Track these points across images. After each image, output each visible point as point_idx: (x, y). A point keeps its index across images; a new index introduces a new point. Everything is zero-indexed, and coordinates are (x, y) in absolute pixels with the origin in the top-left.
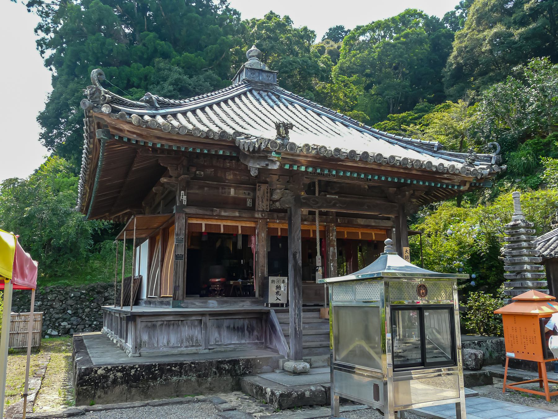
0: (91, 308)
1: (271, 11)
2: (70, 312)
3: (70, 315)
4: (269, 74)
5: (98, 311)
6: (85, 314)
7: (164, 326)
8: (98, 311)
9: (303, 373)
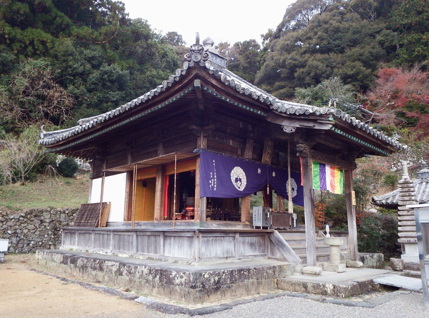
0: (28, 229)
1: (262, 36)
2: (9, 232)
3: (9, 234)
4: (221, 59)
5: (34, 232)
6: (23, 234)
7: (214, 241)
8: (34, 232)
9: (316, 274)
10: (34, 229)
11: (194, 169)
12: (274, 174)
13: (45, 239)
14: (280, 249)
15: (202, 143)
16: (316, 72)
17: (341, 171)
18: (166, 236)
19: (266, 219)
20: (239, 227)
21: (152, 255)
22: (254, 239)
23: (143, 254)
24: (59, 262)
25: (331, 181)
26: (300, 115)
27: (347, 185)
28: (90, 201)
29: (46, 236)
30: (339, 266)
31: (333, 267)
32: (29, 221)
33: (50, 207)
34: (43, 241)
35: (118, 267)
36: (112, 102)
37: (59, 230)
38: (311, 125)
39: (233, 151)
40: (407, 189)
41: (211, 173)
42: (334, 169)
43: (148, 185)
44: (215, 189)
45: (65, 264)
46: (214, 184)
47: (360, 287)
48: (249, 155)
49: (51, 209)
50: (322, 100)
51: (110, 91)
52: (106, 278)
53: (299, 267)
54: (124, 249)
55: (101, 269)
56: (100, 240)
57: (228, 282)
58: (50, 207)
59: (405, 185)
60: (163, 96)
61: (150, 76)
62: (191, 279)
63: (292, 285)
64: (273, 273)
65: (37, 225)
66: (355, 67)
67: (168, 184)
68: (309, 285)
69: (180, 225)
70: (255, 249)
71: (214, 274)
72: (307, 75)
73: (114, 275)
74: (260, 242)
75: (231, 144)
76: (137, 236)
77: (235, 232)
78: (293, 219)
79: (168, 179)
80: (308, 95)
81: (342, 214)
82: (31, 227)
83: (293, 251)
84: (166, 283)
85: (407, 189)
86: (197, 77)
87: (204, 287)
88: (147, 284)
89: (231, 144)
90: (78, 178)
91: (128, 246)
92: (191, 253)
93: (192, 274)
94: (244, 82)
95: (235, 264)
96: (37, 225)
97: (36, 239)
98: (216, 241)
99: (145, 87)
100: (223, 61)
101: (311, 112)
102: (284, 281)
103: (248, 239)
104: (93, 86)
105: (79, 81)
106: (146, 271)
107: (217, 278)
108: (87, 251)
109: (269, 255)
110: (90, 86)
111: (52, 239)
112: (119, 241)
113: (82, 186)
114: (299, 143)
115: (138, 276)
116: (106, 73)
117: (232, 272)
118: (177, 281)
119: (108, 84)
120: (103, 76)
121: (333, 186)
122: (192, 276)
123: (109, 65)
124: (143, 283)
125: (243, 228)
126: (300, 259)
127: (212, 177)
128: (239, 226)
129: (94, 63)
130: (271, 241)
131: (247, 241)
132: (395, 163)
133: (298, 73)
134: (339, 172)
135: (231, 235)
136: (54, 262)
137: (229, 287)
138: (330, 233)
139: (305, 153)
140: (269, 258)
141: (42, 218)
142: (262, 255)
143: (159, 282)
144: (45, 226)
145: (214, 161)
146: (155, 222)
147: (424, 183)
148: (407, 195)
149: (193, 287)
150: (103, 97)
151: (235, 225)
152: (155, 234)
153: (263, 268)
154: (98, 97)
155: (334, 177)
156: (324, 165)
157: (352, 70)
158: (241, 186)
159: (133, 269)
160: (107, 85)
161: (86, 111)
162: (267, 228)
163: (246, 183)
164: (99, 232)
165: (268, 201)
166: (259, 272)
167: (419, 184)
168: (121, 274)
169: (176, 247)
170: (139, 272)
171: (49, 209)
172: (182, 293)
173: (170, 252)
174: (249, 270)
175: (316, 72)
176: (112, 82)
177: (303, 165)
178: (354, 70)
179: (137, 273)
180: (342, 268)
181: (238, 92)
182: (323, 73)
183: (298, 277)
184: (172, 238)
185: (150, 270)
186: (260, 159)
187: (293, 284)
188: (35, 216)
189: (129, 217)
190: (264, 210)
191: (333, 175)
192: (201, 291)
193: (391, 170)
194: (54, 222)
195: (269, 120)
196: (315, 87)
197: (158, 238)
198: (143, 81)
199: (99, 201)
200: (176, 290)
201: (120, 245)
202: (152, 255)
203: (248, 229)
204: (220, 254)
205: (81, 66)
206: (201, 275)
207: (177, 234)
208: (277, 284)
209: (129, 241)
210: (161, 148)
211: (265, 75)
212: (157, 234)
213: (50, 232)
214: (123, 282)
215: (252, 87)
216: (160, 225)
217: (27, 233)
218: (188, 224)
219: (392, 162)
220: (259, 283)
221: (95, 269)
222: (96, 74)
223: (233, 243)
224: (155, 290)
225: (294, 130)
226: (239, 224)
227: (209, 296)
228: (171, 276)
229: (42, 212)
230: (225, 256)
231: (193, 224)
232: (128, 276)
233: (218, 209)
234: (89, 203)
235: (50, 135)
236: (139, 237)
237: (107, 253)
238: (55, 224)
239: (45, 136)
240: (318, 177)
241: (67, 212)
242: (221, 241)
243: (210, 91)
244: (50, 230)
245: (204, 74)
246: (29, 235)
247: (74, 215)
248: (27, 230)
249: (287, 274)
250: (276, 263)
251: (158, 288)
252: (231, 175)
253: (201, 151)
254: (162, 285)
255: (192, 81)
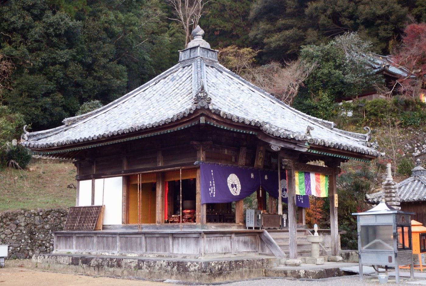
4: (213, 53)
8: (12, 237)
10: (11, 234)
11: (195, 177)
12: (266, 178)
13: (22, 244)
14: (269, 246)
15: (202, 156)
16: (333, 8)
17: (326, 176)
18: (175, 237)
19: (258, 220)
20: (234, 228)
21: (161, 253)
22: (247, 238)
23: (153, 253)
24: (68, 264)
25: (316, 186)
26: (283, 138)
27: (331, 190)
28: (78, 204)
29: (23, 241)
30: (318, 259)
31: (313, 260)
32: (4, 225)
33: (23, 209)
34: (21, 246)
35: (137, 263)
36: (60, 64)
37: (35, 234)
38: (292, 146)
39: (227, 159)
40: (388, 191)
41: (210, 182)
42: (319, 175)
43: (149, 190)
44: (214, 196)
45: (75, 265)
46: (213, 192)
47: (327, 273)
48: (242, 161)
49: (25, 212)
50: (335, 62)
51: (57, 50)
52: (125, 273)
53: (284, 260)
54: (132, 249)
55: (119, 266)
56: (103, 242)
57: (228, 270)
58: (23, 209)
59: (388, 186)
60: (172, 124)
61: (106, 22)
62: (203, 266)
63: (276, 272)
64: (262, 265)
65: (13, 229)
66: (386, 4)
67: (167, 189)
68: (288, 272)
69: (183, 228)
70: (248, 246)
71: (218, 263)
72: (322, 13)
73: (133, 269)
74: (252, 241)
75: (226, 153)
76: (146, 237)
77: (231, 233)
78: (283, 220)
79: (167, 184)
80: (317, 56)
81: (343, 210)
82: (8, 231)
83: (279, 248)
84: (183, 271)
85: (388, 191)
86: (202, 115)
87: (211, 272)
88: (166, 273)
89: (226, 153)
90: (31, 169)
91: (136, 246)
92: (205, 248)
93: (204, 263)
94: (237, 77)
95: (232, 257)
96: (13, 229)
97: (14, 244)
98: (216, 240)
99: (100, 39)
100: (214, 54)
101: (292, 137)
102: (271, 270)
103: (242, 238)
104: (35, 45)
105: (18, 38)
106: (165, 264)
107: (220, 266)
108: (89, 253)
109: (260, 252)
110: (32, 44)
111: (29, 244)
112: (126, 242)
113: (40, 181)
114: (284, 158)
115: (158, 268)
116: (51, 25)
117: (230, 262)
118: (192, 269)
119: (55, 40)
120: (47, 29)
121: (318, 191)
122: (203, 265)
123: (54, 13)
124: (162, 273)
125: (238, 229)
126: (285, 254)
127: (211, 185)
128: (234, 227)
129: (35, 12)
130: (261, 239)
131: (241, 240)
132: (419, 144)
133: (309, 9)
134: (324, 178)
135: (228, 235)
136: (60, 264)
137: (229, 273)
138: (319, 232)
139: (289, 167)
140: (260, 254)
141: (18, 221)
142: (254, 252)
143: (176, 271)
144: (21, 230)
145: (212, 171)
146: (157, 224)
147: (416, 181)
148: (389, 196)
149: (204, 272)
150: (49, 58)
151: (230, 226)
152: (165, 236)
153: (254, 260)
154: (42, 59)
155: (319, 182)
156: (309, 173)
157: (382, 7)
158: (236, 191)
159: (152, 264)
160: (52, 41)
161: (29, 80)
162: (258, 228)
163: (240, 188)
164: (101, 235)
165: (262, 204)
166: (251, 263)
167: (412, 181)
168: (140, 268)
169: (184, 246)
170: (158, 266)
171: (23, 211)
172: (196, 277)
173: (178, 250)
174: (243, 261)
175: (333, 8)
176: (58, 36)
177: (288, 176)
178: (386, 8)
179: (156, 266)
180: (320, 261)
181: (234, 122)
182: (343, 11)
183: (282, 267)
184: (180, 239)
185: (168, 263)
186: (252, 163)
187: (277, 272)
188: (11, 220)
189: (127, 220)
190: (256, 213)
191: (318, 180)
192: (209, 275)
193: (414, 154)
194: (29, 225)
195: (259, 138)
196: (326, 45)
197: (167, 239)
198: (98, 31)
199: (89, 204)
200: (191, 275)
201: (127, 246)
202: (161, 253)
203: (242, 230)
204: (219, 250)
205: (20, 18)
206: (209, 264)
207: (185, 236)
208: (265, 273)
209: (136, 243)
210: (160, 156)
211: (265, 7)
212: (166, 235)
213: (26, 237)
214: (143, 274)
215: (245, 83)
216: (163, 228)
217: (4, 238)
218: (191, 227)
219: (416, 144)
220: (250, 271)
221: (112, 266)
222: (38, 29)
223: (229, 242)
224: (174, 276)
225: (279, 149)
226: (234, 226)
227: (215, 278)
228: (186, 266)
229: (16, 215)
230: (224, 252)
231: (195, 227)
232: (148, 269)
233: (212, 210)
234: (77, 206)
235: (34, 136)
236: (148, 239)
237: (114, 254)
238: (31, 228)
239: (29, 137)
240: (304, 184)
241: (41, 214)
242: (221, 240)
243: (212, 124)
244: (27, 234)
245: (208, 113)
246: (7, 241)
247: (49, 216)
248: (4, 235)
249: (274, 266)
250: (264, 257)
251: (176, 275)
252: (228, 182)
253: (201, 163)
254: (179, 273)
255: (198, 118)
